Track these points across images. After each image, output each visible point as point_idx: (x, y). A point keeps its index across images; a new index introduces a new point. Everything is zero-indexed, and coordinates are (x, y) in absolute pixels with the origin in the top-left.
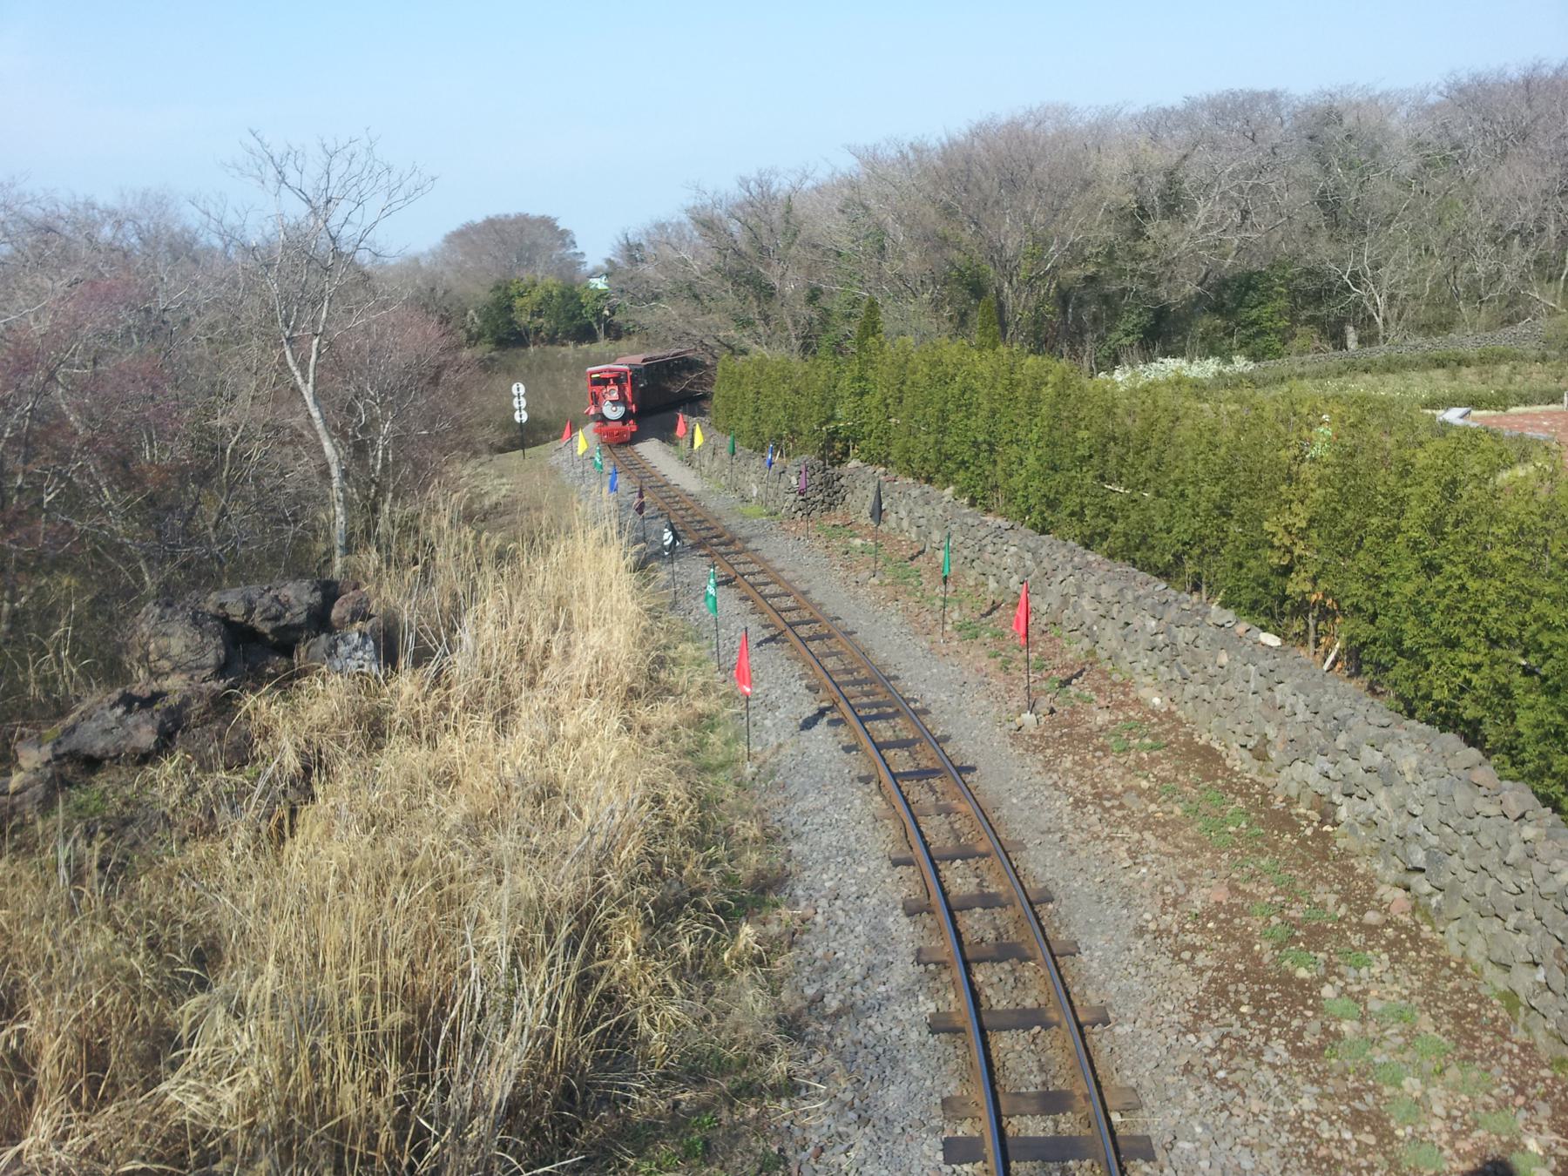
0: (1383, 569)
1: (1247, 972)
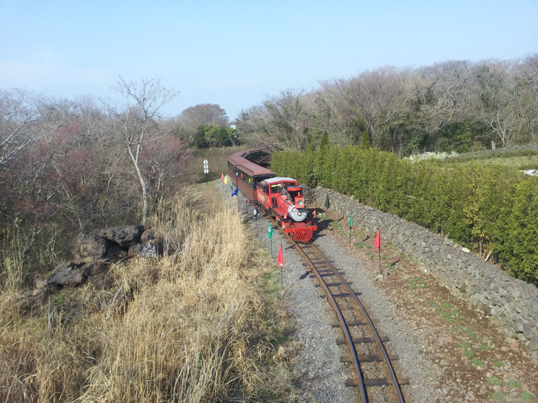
0: (506, 226)
1: (459, 367)
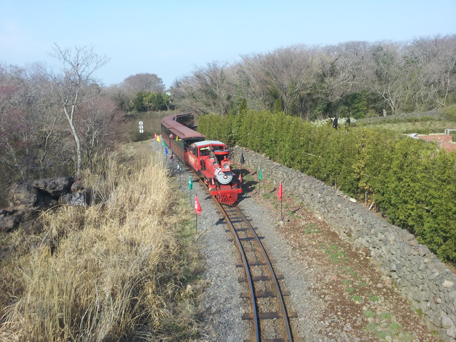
0: (386, 180)
1: (340, 302)
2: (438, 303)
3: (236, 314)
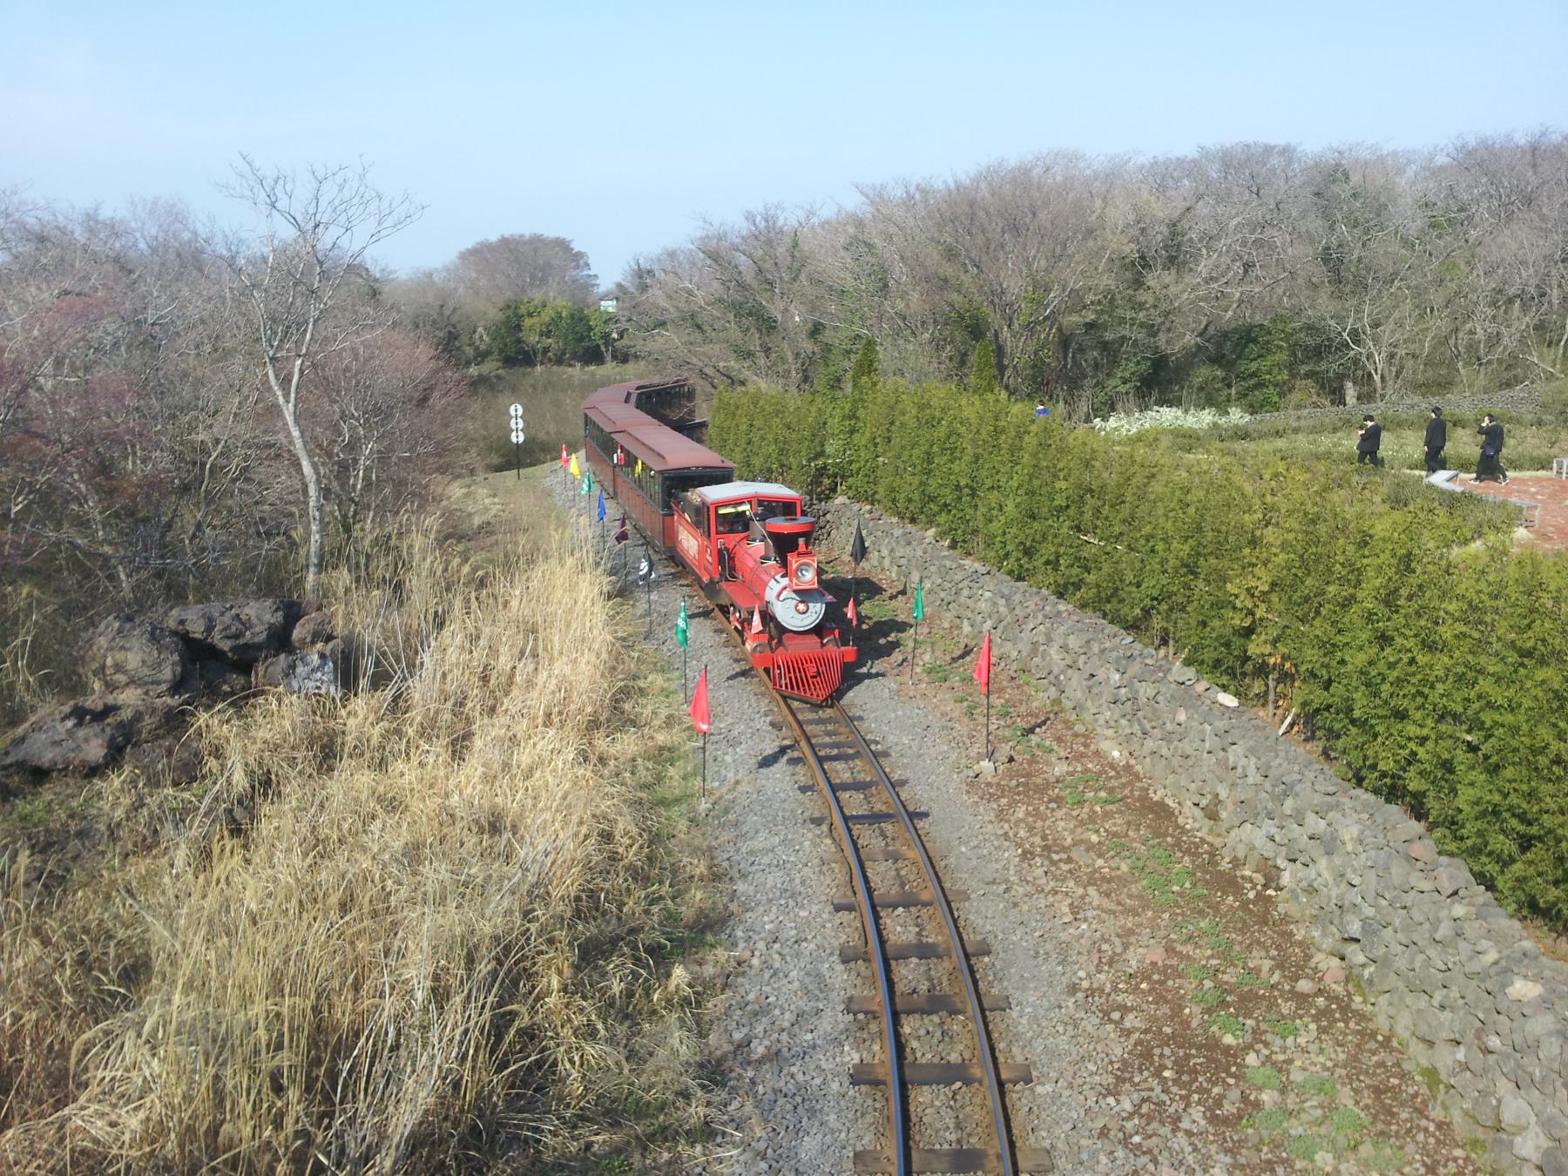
1: (1173, 1036)
2: (1492, 1052)
3: (831, 1066)
